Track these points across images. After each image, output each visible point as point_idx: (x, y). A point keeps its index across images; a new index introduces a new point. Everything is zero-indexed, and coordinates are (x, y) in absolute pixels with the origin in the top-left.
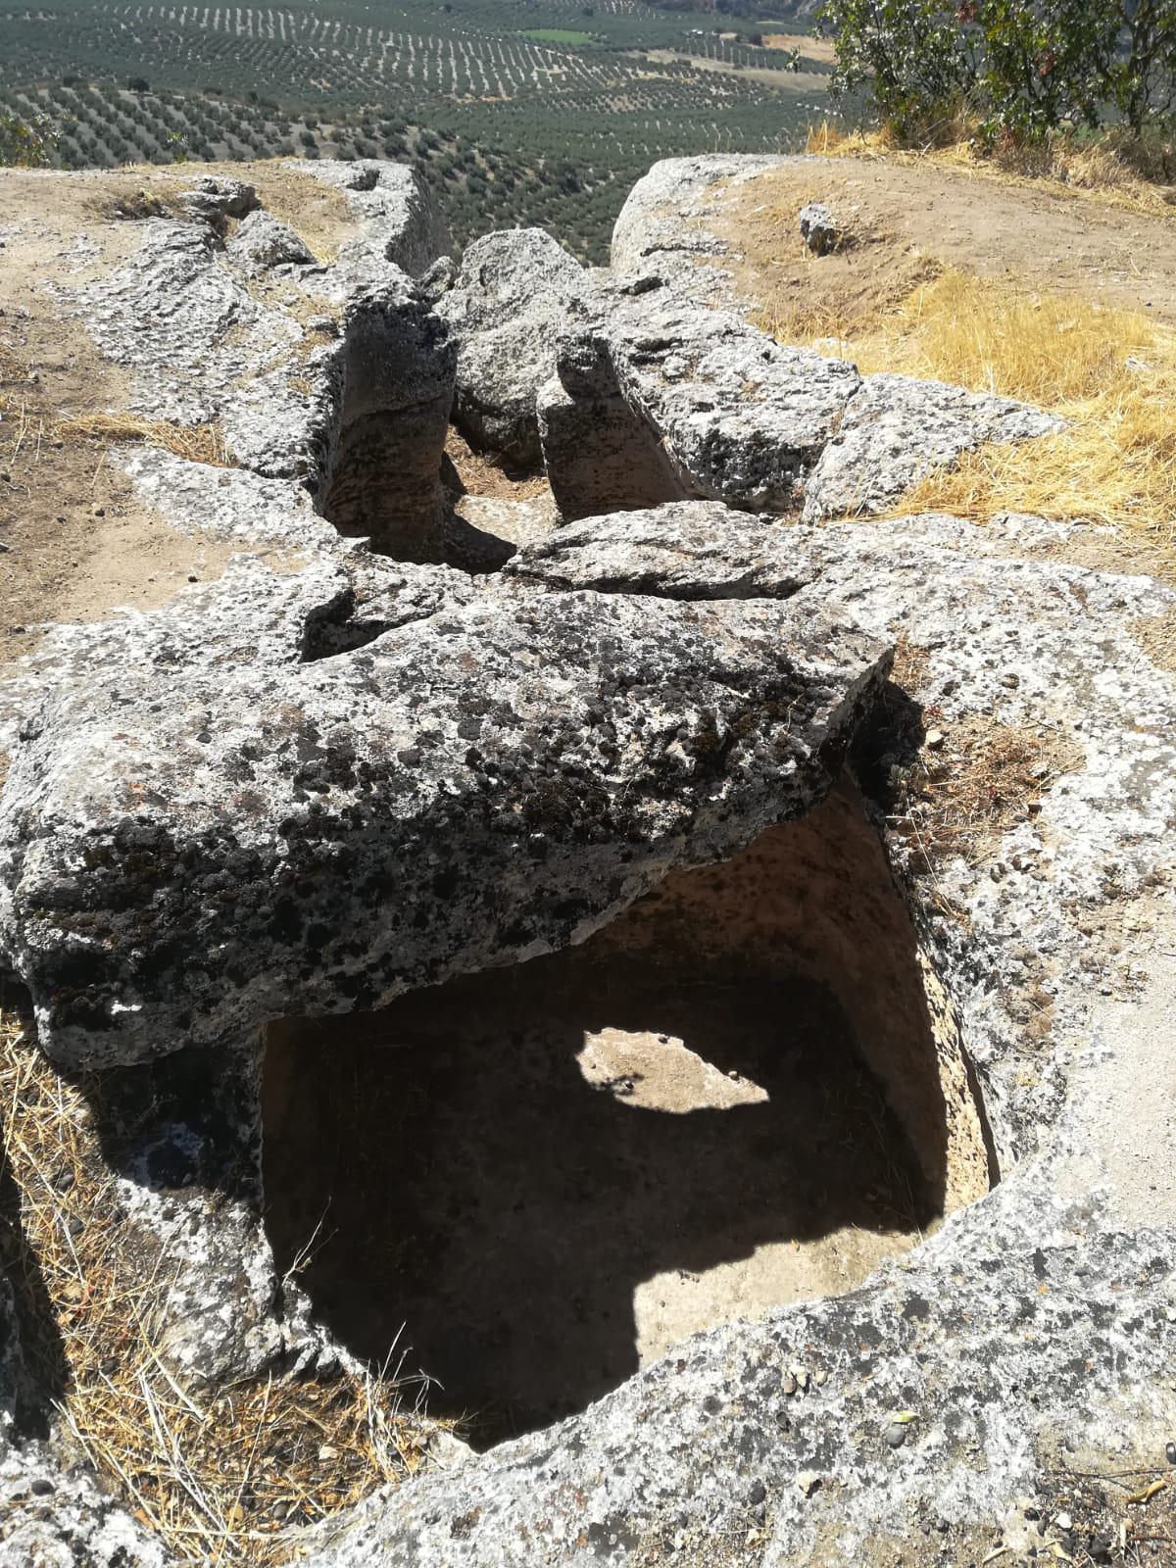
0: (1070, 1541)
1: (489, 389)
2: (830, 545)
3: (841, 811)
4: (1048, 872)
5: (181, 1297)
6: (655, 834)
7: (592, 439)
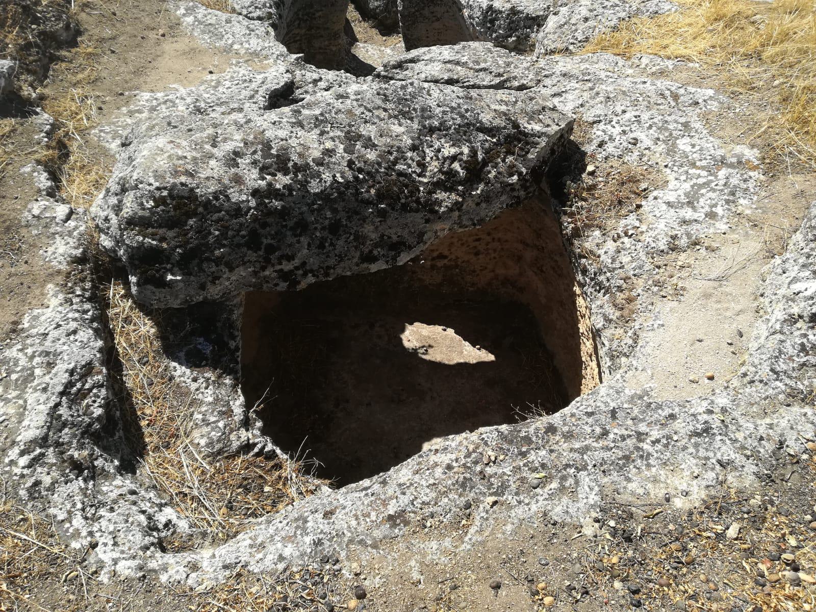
0: (614, 532)
2: (546, 67)
3: (542, 214)
4: (642, 238)
5: (200, 416)
6: (443, 209)
7: (426, 12)
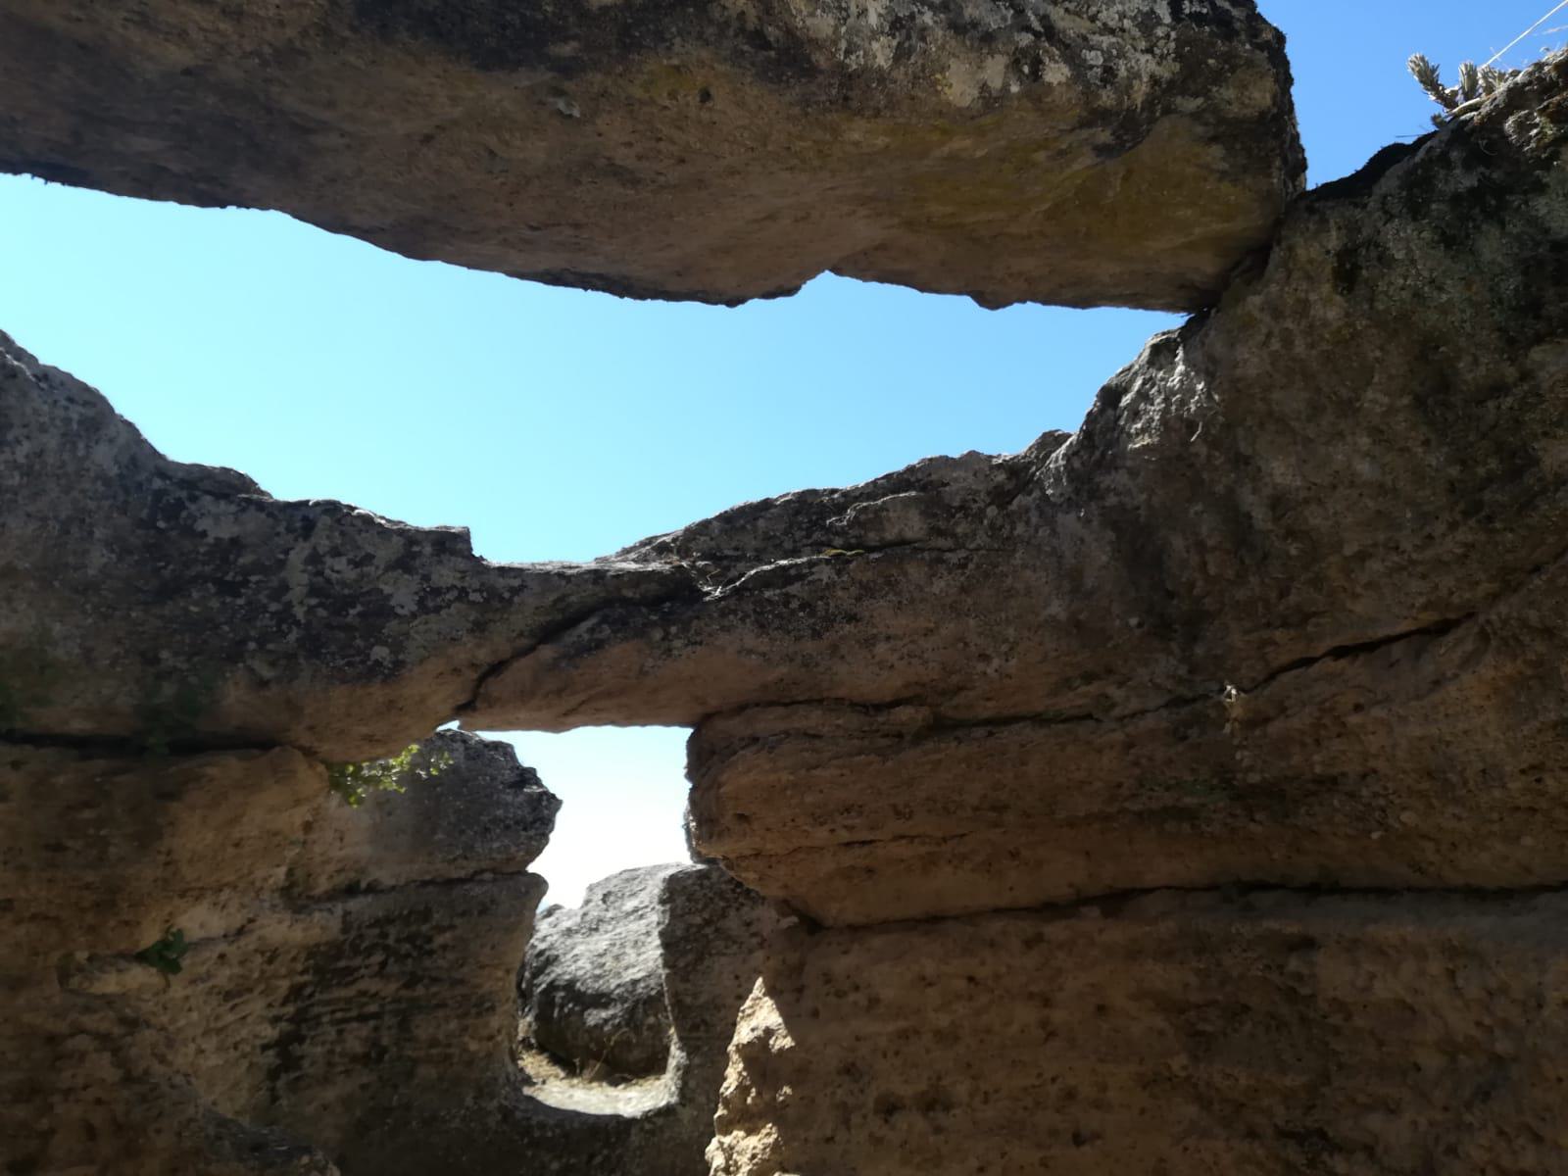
1: (599, 977)
7: (732, 923)
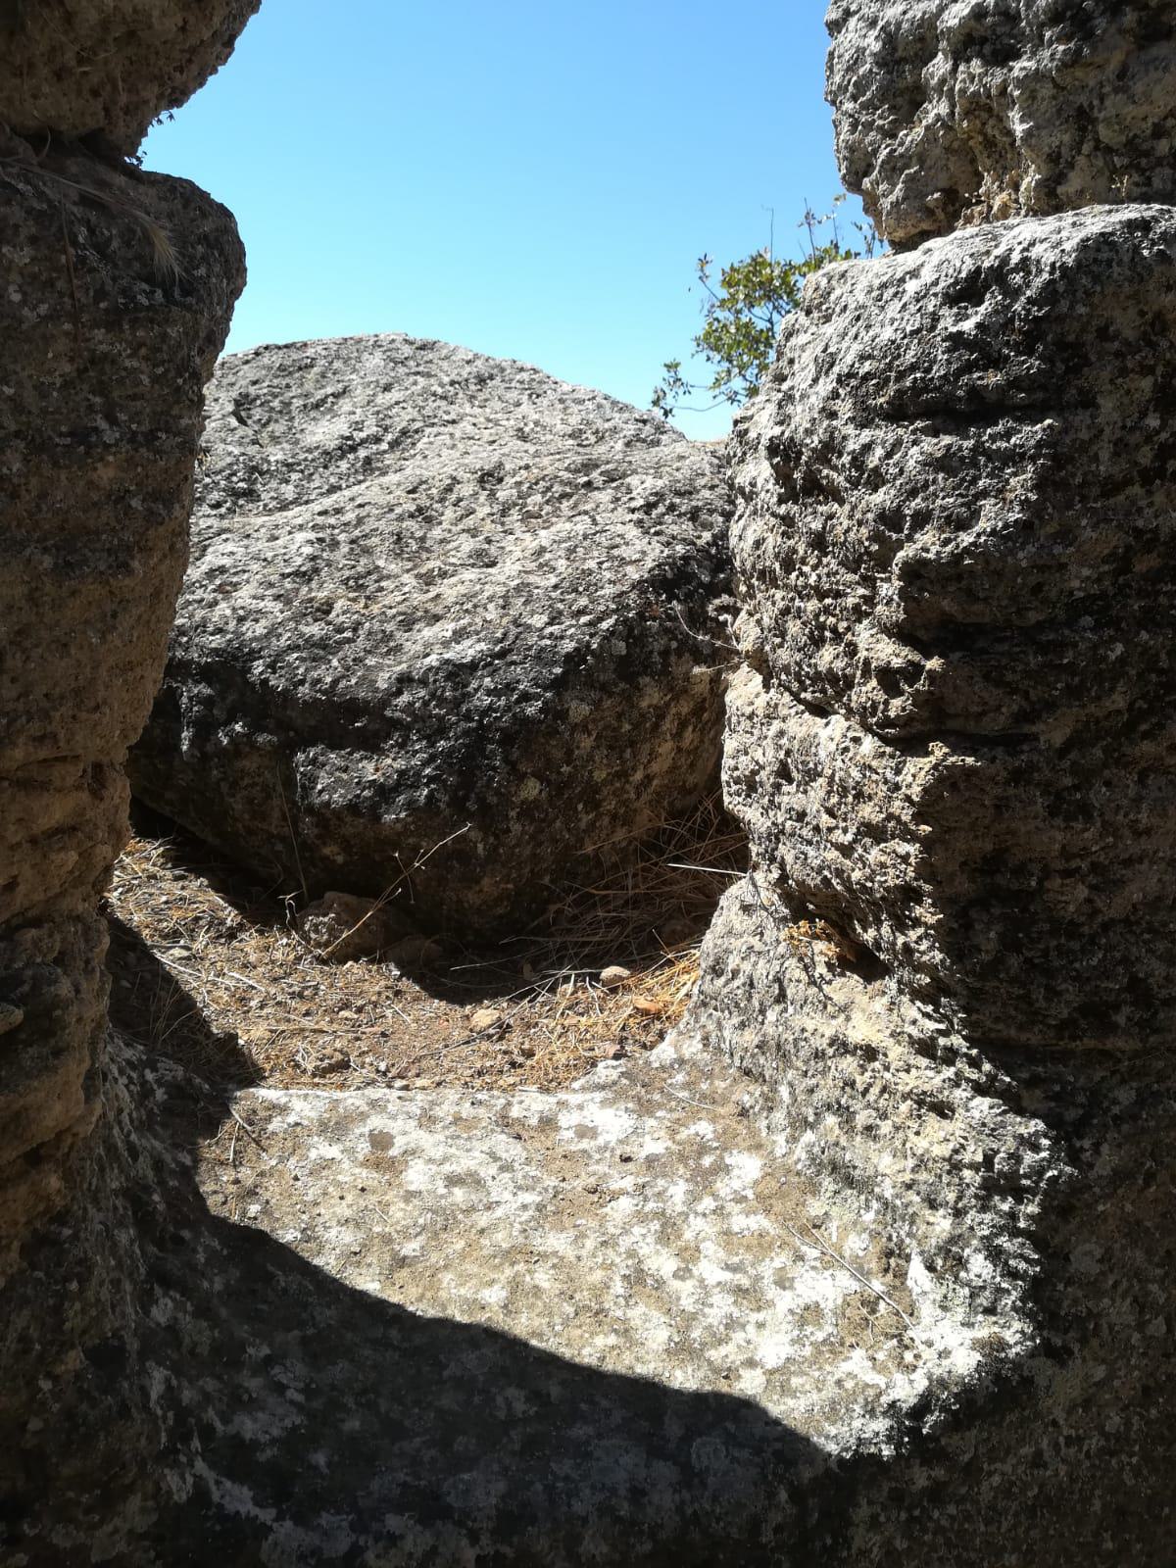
1: (321, 649)
